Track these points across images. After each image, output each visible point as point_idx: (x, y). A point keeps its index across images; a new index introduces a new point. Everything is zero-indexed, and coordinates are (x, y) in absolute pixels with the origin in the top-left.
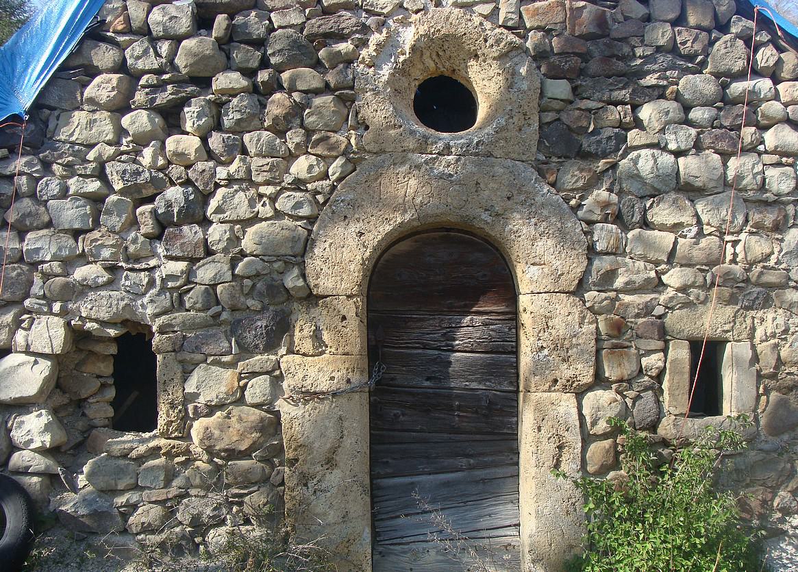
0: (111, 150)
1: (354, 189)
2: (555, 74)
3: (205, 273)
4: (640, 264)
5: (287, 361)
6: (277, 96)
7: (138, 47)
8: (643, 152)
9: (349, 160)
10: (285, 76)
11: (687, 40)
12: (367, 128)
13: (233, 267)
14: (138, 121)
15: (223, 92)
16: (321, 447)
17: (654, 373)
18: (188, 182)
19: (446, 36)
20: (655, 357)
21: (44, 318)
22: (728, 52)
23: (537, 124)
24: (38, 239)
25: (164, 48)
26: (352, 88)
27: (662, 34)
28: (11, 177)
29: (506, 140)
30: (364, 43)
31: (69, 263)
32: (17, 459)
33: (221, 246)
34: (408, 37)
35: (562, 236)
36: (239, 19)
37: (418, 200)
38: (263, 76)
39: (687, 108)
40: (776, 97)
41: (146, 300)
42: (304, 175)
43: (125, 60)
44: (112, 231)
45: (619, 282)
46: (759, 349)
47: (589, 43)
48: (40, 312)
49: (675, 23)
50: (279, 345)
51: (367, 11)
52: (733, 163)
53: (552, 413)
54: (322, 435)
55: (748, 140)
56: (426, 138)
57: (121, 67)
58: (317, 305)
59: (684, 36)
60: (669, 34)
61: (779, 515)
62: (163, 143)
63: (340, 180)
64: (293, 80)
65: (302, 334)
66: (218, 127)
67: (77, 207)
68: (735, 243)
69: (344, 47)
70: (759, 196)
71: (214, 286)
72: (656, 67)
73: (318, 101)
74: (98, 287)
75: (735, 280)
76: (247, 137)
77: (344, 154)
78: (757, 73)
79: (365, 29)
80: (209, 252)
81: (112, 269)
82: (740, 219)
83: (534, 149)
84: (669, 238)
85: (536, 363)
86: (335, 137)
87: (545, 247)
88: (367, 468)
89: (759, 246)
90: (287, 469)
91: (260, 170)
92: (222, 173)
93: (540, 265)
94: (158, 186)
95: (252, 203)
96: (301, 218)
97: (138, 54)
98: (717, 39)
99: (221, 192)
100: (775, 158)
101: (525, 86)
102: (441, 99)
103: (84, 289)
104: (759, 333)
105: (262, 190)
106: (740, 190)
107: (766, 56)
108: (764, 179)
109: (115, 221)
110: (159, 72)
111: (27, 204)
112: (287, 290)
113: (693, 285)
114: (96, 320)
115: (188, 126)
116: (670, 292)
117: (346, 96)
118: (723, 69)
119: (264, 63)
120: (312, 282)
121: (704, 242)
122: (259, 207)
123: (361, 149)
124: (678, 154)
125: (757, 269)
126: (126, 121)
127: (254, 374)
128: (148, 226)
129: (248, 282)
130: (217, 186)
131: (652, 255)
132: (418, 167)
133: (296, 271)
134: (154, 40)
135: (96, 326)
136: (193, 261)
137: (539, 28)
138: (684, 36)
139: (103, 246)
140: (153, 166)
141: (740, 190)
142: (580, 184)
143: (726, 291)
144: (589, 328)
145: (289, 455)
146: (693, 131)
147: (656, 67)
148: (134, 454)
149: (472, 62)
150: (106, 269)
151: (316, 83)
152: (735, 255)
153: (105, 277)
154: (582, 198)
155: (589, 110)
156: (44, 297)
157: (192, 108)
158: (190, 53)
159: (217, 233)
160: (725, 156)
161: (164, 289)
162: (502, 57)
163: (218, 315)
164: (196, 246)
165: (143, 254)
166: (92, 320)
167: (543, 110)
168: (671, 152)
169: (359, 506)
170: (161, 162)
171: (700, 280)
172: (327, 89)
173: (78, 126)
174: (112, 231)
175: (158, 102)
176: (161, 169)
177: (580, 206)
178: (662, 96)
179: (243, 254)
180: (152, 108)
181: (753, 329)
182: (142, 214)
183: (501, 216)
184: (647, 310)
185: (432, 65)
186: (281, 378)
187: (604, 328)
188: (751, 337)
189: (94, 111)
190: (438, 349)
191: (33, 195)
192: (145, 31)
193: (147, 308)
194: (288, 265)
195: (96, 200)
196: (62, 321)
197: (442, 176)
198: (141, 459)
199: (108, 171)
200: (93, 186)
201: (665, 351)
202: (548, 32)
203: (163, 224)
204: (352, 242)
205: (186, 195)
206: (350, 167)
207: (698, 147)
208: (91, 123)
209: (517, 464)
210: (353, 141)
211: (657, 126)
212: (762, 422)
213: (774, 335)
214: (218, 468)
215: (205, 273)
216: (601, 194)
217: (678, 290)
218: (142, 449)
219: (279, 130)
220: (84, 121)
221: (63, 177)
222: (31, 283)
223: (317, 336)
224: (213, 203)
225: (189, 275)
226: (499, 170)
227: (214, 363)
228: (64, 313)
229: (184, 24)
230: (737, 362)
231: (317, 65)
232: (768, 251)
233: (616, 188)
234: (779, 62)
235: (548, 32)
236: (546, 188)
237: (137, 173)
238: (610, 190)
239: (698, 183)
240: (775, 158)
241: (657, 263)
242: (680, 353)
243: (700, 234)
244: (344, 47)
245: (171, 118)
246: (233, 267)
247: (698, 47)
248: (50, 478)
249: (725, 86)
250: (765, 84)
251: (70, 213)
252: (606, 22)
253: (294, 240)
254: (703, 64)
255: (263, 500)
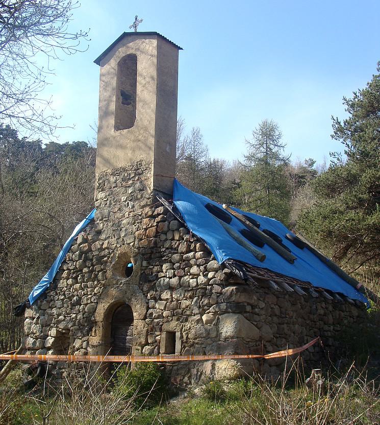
18: (77, 296)
67: (302, 387)
81: (65, 317)
84: (165, 302)
110: (74, 269)
144: (146, 329)
167: (141, 270)
183: (130, 300)
242: (164, 335)
251: (59, 303)
252: (156, 243)
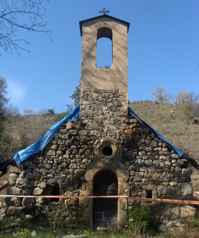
0: (55, 157)
1: (92, 164)
2: (125, 147)
3: (68, 177)
4: (138, 178)
5: (81, 191)
6: (81, 149)
7: (60, 141)
8: (139, 159)
9: (92, 160)
10: (82, 146)
11: (147, 141)
12: (95, 155)
13: (73, 176)
14: (59, 152)
15: (72, 148)
16: (85, 205)
17: (140, 195)
18: (66, 162)
19: (108, 141)
20: (140, 193)
21: (43, 182)
22: (154, 143)
23: (122, 155)
24: (42, 170)
25: (64, 141)
26: (93, 149)
27: (143, 141)
28: (39, 160)
29: (117, 157)
30: (95, 142)
31: (47, 174)
32: (36, 204)
33: (71, 172)
34: (102, 140)
35: (125, 173)
36: (75, 137)
37: (102, 167)
38: (79, 146)
39: (147, 152)
40: (162, 151)
41: (59, 180)
42: (85, 162)
43: (57, 143)
44: (54, 169)
45: (134, 180)
46: (158, 192)
47: (130, 142)
48: (42, 181)
49: (145, 139)
50: (79, 189)
51: (96, 137)
52: (154, 162)
53: (123, 201)
54: (86, 203)
55: (157, 158)
56: (104, 157)
57: (57, 144)
58: (86, 182)
59: (147, 141)
60: (144, 141)
61: (161, 220)
62: (63, 156)
63: (90, 163)
64: (83, 147)
65: (83, 187)
66: (71, 154)
68: (154, 175)
69: (92, 142)
70: (158, 167)
71: (70, 179)
72: (141, 146)
73: (87, 150)
74: (51, 178)
75: (154, 180)
76: (76, 156)
77: (91, 159)
78: (158, 147)
79: (95, 139)
80: (69, 173)
81: (54, 175)
82: (155, 171)
83: (121, 159)
85: (120, 193)
86: (90, 156)
87: (122, 174)
88: (92, 209)
89: (158, 175)
90: (80, 208)
91: (78, 161)
92: (72, 161)
93: (121, 177)
94: (62, 162)
95: (76, 166)
96: (84, 169)
97: (59, 142)
98: (152, 141)
99: (71, 164)
100: (161, 161)
101: (120, 149)
102: (106, 150)
103: (49, 178)
104: (158, 189)
105: (78, 164)
106: (156, 166)
107: (160, 144)
108: (159, 164)
109: (55, 168)
111: (41, 164)
112: (81, 180)
113: (147, 181)
114: (51, 183)
115: (67, 153)
116: (143, 182)
117: (92, 150)
118: (153, 146)
119: (79, 144)
120: (85, 179)
121: (149, 174)
122: (77, 167)
123: (94, 158)
124: (145, 160)
125: (158, 179)
126: (57, 152)
127: (75, 193)
128: (60, 169)
129: (75, 178)
130: (71, 163)
131: (140, 176)
132: (102, 161)
133: (83, 177)
134: (62, 140)
135: (51, 184)
136: (66, 174)
137: (123, 140)
138: (147, 141)
139: (52, 171)
140: (61, 159)
141: (156, 166)
142: (128, 164)
143: (152, 182)
145: (80, 206)
146: (147, 156)
147: (141, 146)
148: (55, 204)
149: (112, 145)
150: (53, 175)
151: (87, 148)
152: (154, 176)
153: (53, 176)
154: (129, 167)
155: (130, 153)
156: (43, 179)
157: (68, 151)
158: (67, 142)
159: (70, 170)
160: (153, 160)
161: (62, 179)
162: (116, 144)
163: (70, 183)
164: (67, 172)
165: (59, 173)
166: (50, 183)
167: (123, 153)
168: (144, 160)
169: (91, 214)
170: (62, 159)
171: (148, 180)
172: (89, 149)
173: (50, 152)
174: (54, 169)
175: (62, 149)
176: (63, 160)
177: (128, 168)
178: (143, 151)
179: (74, 174)
180: (61, 150)
181: (157, 189)
182: (59, 167)
183: (116, 169)
184: (139, 185)
185: (105, 145)
186: (79, 193)
187: (174, 201)
188: (157, 190)
189: (52, 150)
190: (105, 191)
191: (42, 163)
192: (61, 138)
193: (59, 182)
194: (82, 176)
195: (52, 164)
196: (45, 183)
197: (106, 163)
198: (56, 205)
199: (54, 160)
200: (52, 162)
201: (142, 192)
202: (124, 140)
203: (62, 168)
204: (92, 173)
205: (66, 164)
206: (92, 161)
207: (148, 159)
208: (52, 152)
209: (117, 210)
210: (92, 157)
211: (141, 155)
212: (158, 204)
213: (160, 190)
214: (68, 207)
215: (68, 177)
216: (132, 166)
217: (144, 182)
218: (57, 204)
219: (81, 155)
220: (51, 152)
221: (47, 160)
222: (41, 177)
223: (85, 187)
224: (70, 166)
225: (66, 176)
226: (115, 162)
227: (69, 191)
228: (46, 182)
229: (67, 138)
230: (154, 194)
231: (87, 145)
232: (160, 176)
233: (134, 165)
234: (162, 145)
235: (124, 140)
236: (123, 165)
237: (59, 160)
238: (133, 166)
239: (148, 165)
240: (161, 161)
241: (141, 177)
243: (148, 173)
244: (92, 142)
245: (64, 152)
246: (73, 176)
247: (149, 142)
248: (41, 208)
249: (153, 149)
250: (160, 148)
251: (48, 166)
253: (83, 172)
254: (150, 145)
255: (76, 213)
